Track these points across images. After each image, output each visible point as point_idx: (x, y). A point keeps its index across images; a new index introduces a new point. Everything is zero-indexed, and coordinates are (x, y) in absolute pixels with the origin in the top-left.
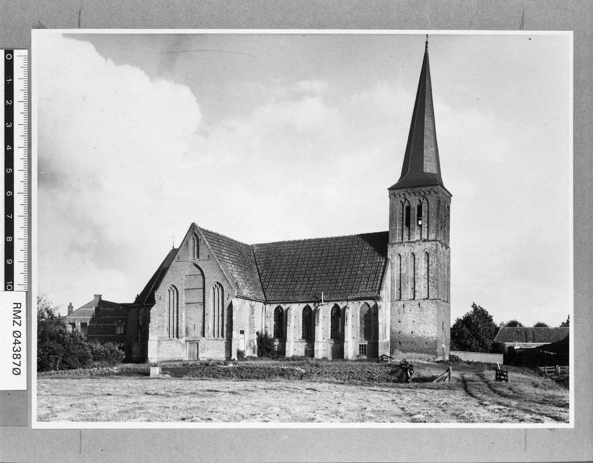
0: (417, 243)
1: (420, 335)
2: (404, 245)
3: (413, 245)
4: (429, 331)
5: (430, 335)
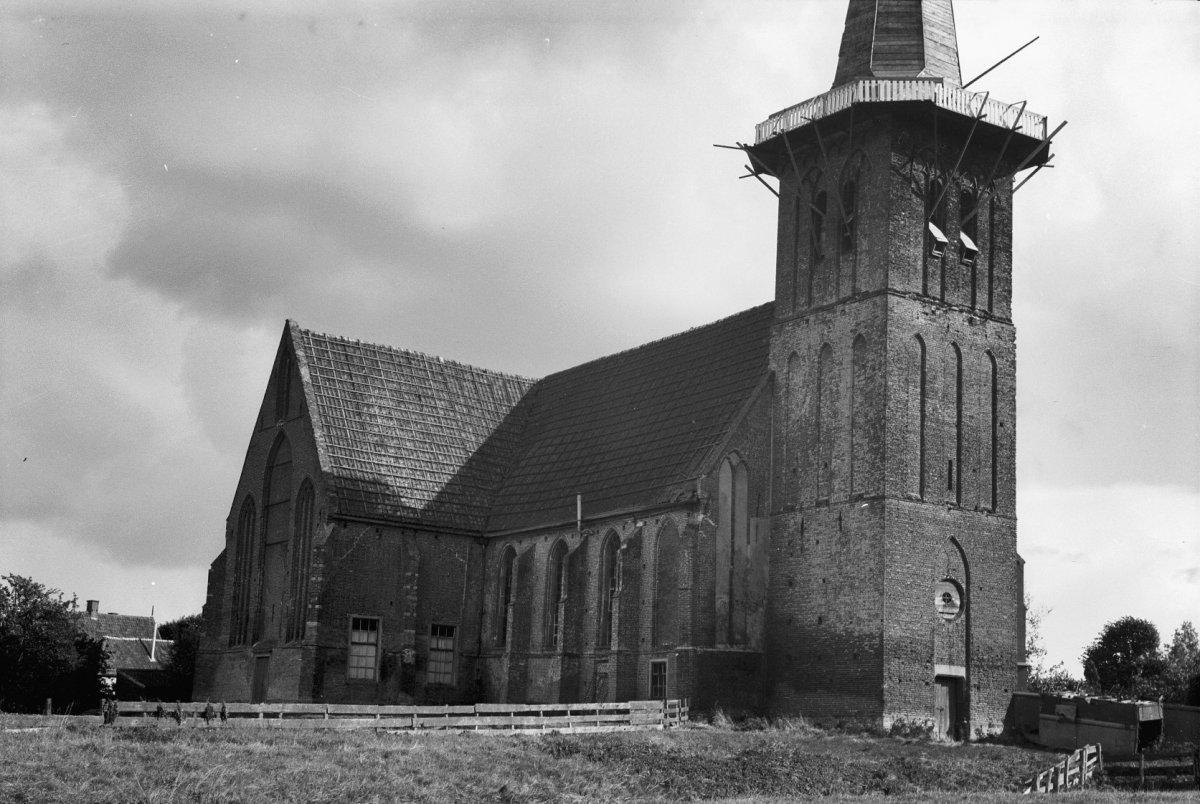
0: (840, 308)
1: (840, 627)
2: (807, 321)
3: (829, 316)
4: (863, 615)
5: (866, 630)
